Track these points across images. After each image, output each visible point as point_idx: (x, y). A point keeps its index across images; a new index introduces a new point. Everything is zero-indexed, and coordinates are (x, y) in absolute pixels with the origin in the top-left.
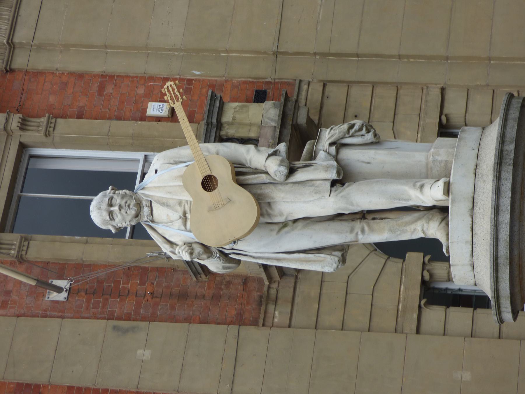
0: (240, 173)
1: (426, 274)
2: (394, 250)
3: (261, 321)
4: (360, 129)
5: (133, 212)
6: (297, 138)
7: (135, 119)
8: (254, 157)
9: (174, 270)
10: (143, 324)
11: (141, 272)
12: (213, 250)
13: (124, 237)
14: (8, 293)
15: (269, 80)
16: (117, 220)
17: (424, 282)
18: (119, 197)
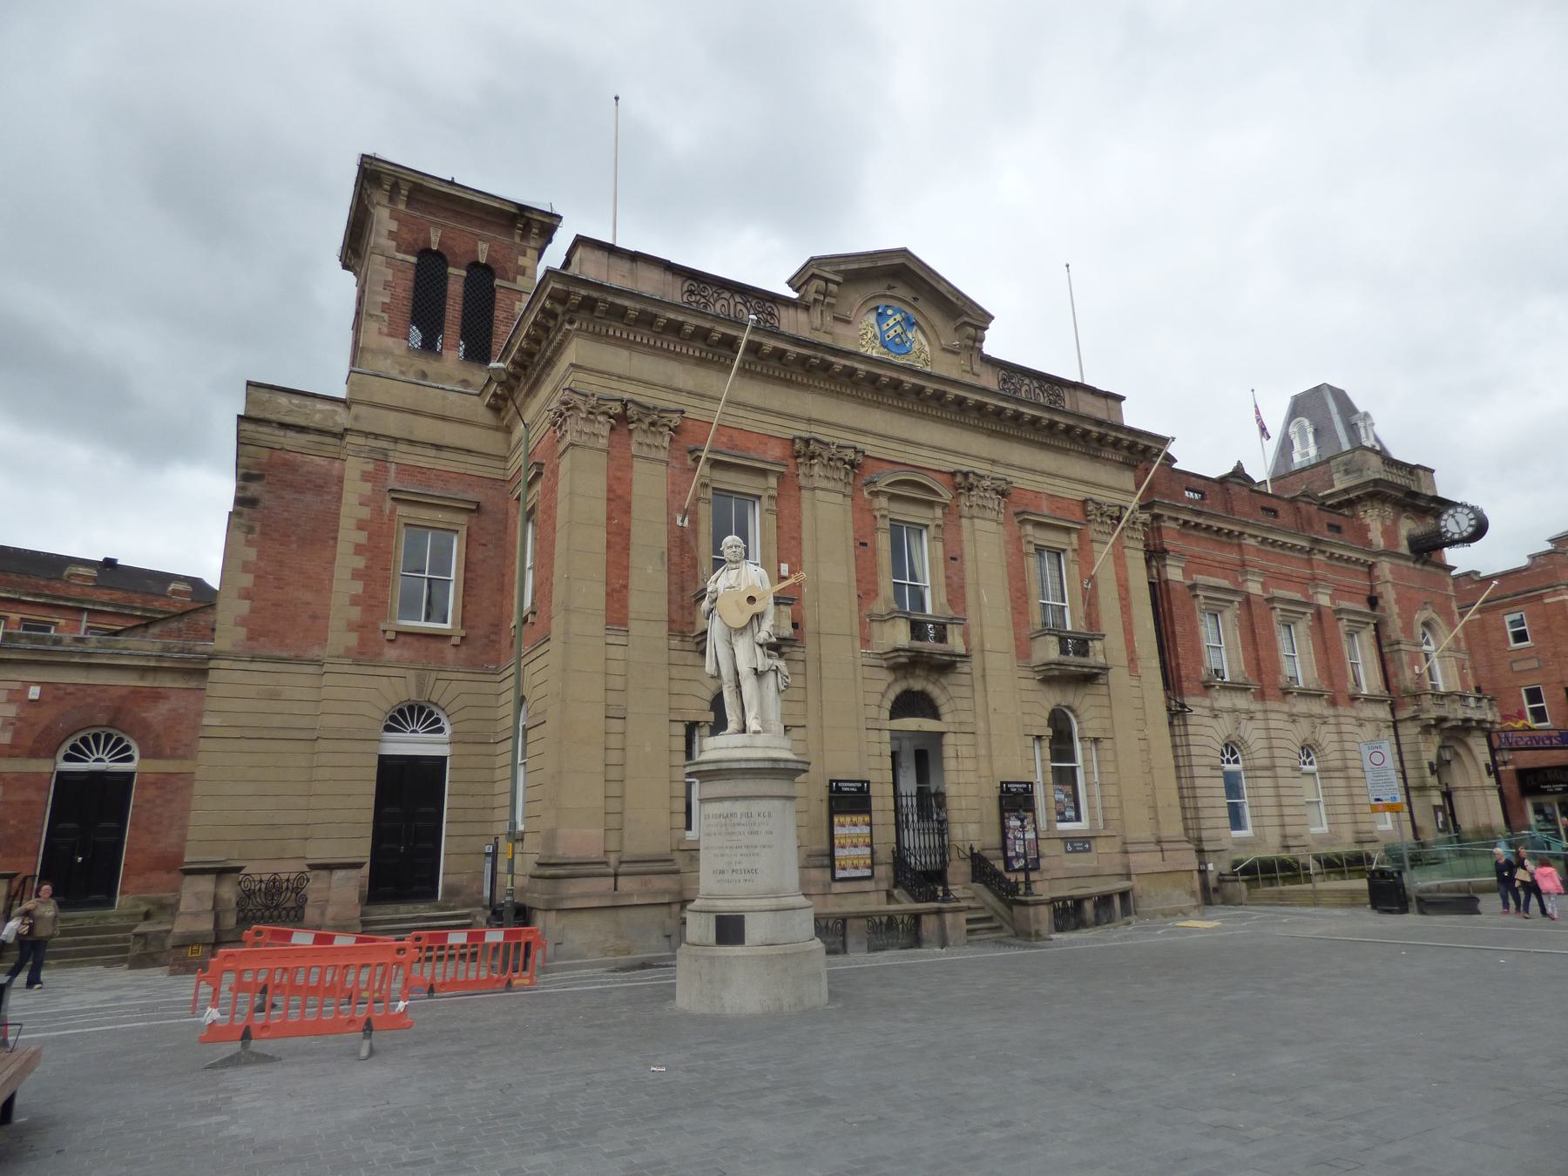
0: (758, 617)
2: (717, 703)
6: (775, 647)
8: (767, 625)
11: (694, 565)
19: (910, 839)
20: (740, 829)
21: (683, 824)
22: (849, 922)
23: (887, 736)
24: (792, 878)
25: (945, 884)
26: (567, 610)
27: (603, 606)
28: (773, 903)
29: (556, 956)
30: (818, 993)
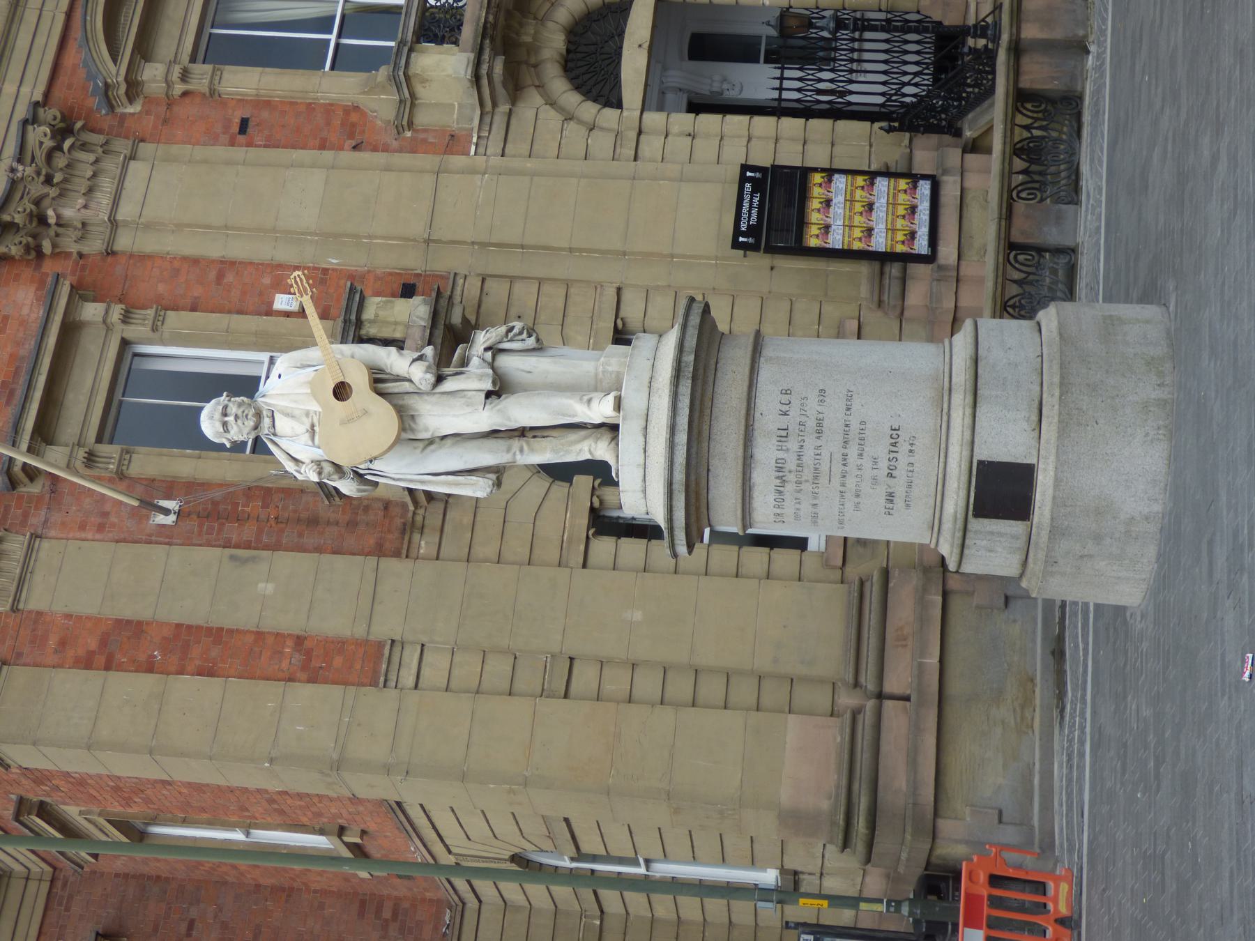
0: (379, 380)
1: (595, 500)
2: (560, 472)
3: (404, 552)
4: (521, 333)
5: (251, 423)
6: (449, 339)
7: (259, 314)
9: (302, 491)
10: (265, 554)
12: (346, 469)
13: (244, 451)
14: (105, 514)
15: (419, 271)
16: (232, 432)
17: (592, 510)
18: (235, 405)
19: (867, 93)
20: (809, 454)
21: (794, 554)
22: (1017, 237)
23: (654, 119)
24: (915, 357)
25: (962, 32)
26: (338, 765)
27: (337, 691)
28: (960, 400)
29: (1024, 822)
30: (1143, 324)
